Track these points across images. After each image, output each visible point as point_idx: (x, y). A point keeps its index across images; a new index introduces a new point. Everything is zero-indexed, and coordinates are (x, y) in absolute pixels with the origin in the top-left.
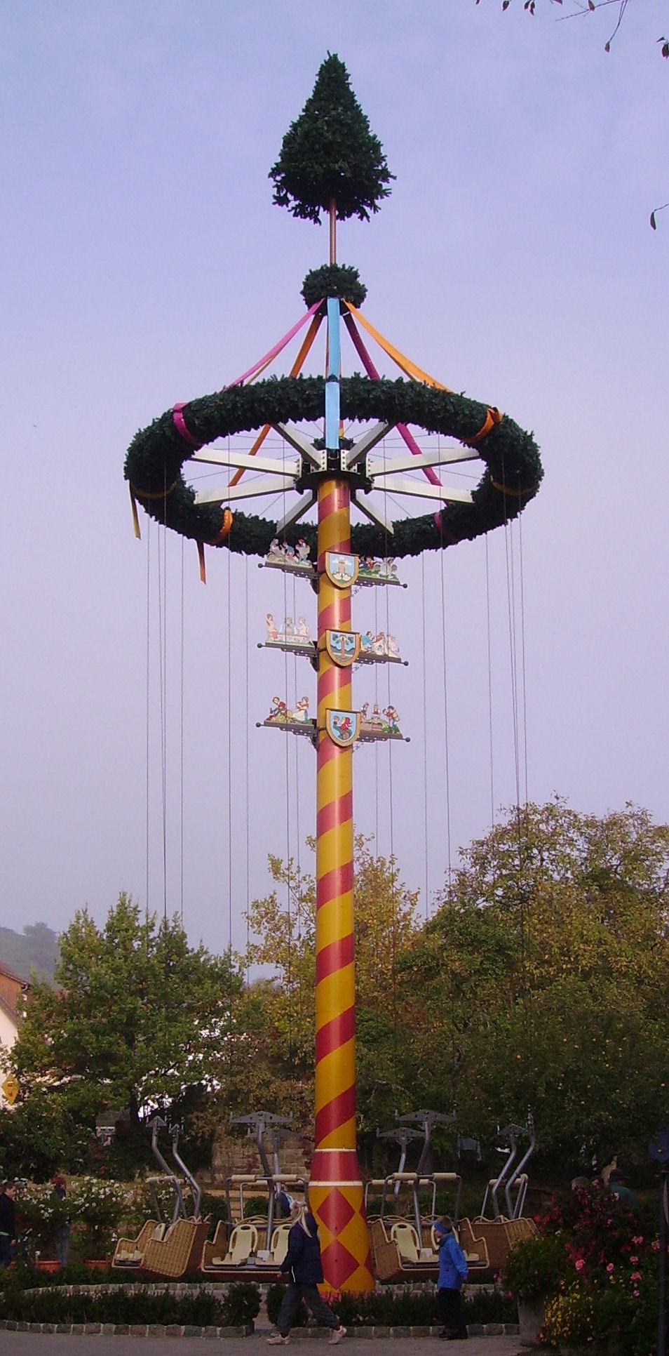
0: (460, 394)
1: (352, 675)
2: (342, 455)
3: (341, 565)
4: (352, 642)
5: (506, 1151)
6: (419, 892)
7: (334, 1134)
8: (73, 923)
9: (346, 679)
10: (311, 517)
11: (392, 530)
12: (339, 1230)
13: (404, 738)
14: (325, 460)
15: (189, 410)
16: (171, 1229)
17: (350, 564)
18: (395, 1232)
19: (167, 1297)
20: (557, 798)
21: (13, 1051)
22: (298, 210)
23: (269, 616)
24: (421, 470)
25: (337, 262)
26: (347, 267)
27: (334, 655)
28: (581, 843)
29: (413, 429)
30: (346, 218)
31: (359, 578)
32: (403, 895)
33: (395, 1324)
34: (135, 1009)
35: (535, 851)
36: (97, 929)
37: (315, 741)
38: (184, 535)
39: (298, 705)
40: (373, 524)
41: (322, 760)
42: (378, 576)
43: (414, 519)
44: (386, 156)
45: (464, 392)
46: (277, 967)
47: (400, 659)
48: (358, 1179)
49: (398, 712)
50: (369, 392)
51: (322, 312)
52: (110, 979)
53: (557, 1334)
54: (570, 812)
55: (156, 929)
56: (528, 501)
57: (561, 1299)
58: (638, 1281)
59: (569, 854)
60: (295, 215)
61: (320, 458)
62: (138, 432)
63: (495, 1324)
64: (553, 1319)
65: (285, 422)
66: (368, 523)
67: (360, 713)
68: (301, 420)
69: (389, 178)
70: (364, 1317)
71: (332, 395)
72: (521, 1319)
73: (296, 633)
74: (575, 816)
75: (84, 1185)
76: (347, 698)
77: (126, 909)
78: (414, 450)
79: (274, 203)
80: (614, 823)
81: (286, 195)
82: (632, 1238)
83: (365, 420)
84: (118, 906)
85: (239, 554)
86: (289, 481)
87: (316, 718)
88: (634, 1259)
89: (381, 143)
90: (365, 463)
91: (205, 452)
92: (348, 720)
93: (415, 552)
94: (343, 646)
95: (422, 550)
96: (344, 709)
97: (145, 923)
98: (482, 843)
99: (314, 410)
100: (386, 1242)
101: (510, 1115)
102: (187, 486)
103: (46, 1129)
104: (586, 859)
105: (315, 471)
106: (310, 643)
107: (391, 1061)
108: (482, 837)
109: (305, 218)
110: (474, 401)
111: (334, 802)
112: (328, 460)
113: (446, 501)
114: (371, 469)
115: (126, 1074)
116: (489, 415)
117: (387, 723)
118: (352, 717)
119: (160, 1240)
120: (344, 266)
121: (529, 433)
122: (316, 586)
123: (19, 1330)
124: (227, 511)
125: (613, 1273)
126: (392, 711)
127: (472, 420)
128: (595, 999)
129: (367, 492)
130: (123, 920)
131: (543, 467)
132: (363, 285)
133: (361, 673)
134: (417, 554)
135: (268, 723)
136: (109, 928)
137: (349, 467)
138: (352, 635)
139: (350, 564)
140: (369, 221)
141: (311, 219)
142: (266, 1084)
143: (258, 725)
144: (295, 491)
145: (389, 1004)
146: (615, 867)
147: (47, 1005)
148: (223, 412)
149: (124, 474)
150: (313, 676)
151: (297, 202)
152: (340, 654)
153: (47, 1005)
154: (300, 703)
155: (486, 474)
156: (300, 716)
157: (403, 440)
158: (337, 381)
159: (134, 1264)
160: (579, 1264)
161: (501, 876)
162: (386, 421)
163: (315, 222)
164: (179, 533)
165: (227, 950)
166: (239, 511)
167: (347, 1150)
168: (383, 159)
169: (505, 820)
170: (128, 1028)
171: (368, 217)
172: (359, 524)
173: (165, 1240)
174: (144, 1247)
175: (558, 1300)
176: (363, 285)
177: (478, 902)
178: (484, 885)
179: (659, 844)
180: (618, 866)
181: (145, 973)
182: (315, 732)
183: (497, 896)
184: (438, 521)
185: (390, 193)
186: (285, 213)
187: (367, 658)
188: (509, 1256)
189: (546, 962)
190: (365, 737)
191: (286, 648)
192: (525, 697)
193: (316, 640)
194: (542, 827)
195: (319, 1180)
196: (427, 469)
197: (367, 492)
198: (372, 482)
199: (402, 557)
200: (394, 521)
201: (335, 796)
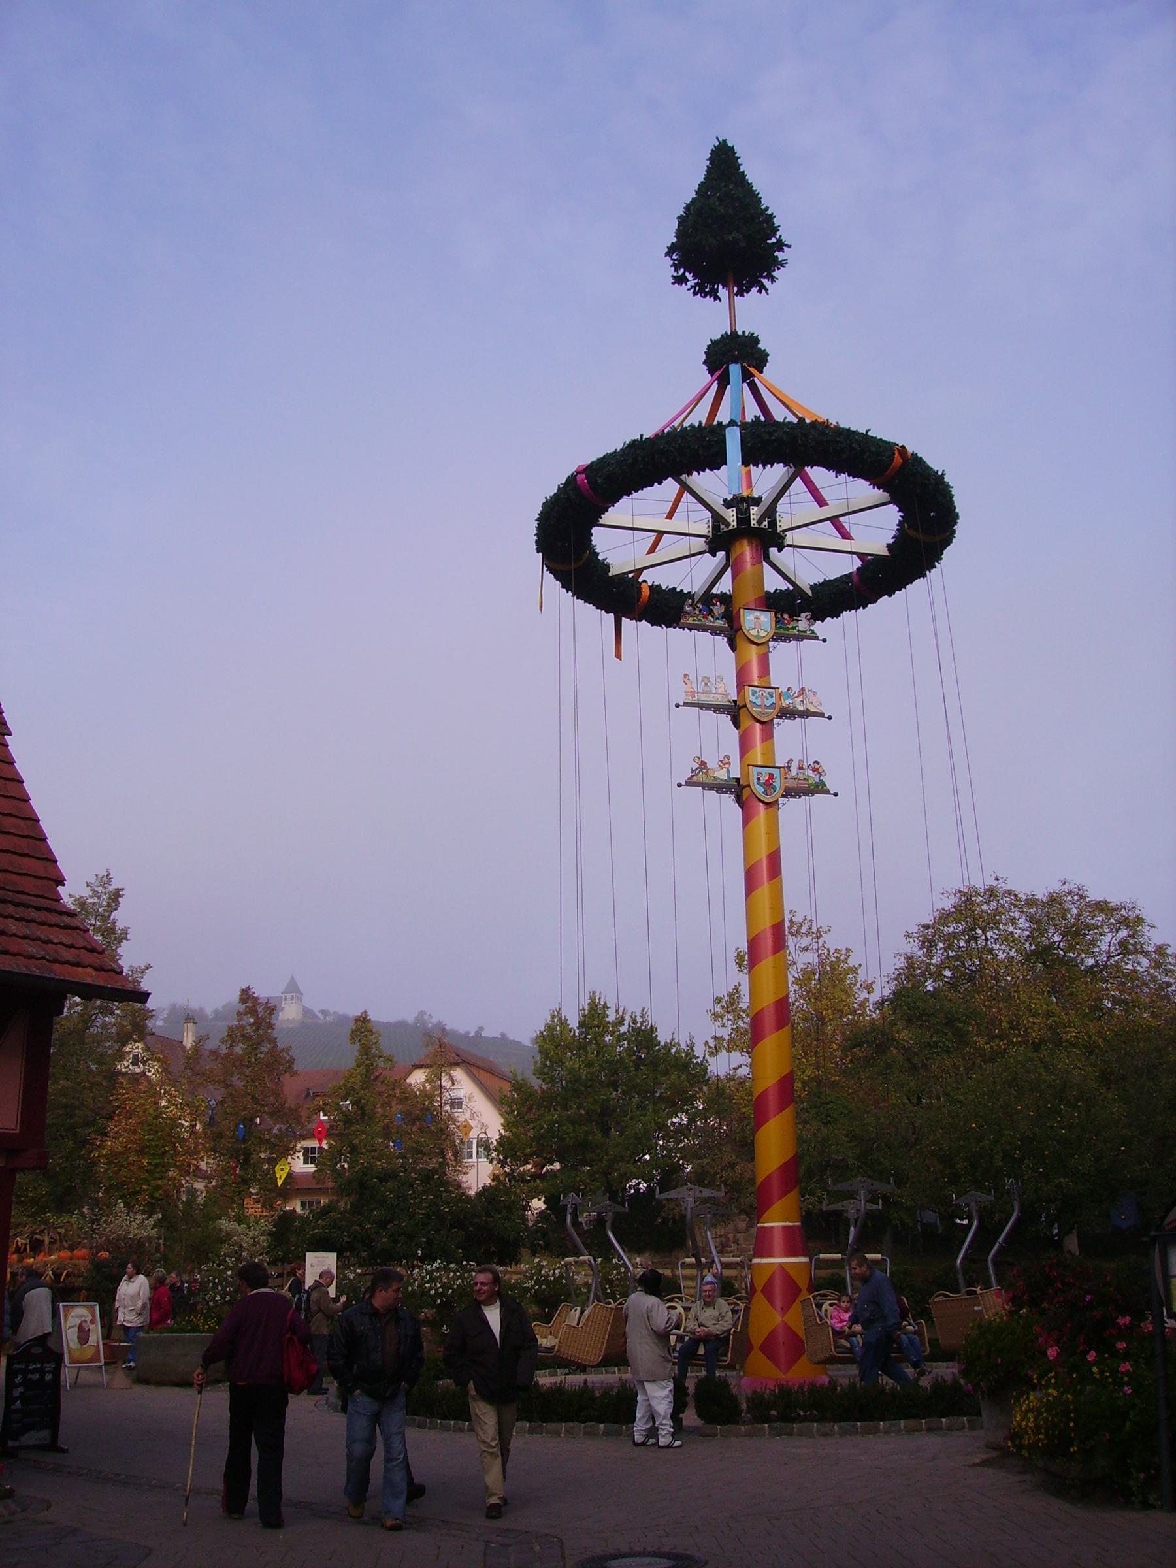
0: (865, 432)
1: (775, 731)
2: (752, 512)
3: (757, 622)
4: (772, 697)
5: (965, 1222)
6: (874, 982)
7: (777, 1208)
8: (548, 1022)
9: (768, 735)
10: (725, 586)
11: (810, 593)
12: (785, 1310)
13: (832, 792)
14: (735, 518)
15: (592, 470)
16: (586, 1312)
17: (766, 620)
18: (826, 1310)
19: (585, 1389)
20: (997, 879)
21: (498, 1143)
22: (697, 288)
23: (686, 675)
24: (829, 522)
25: (737, 329)
26: (747, 334)
27: (755, 711)
28: (1023, 923)
29: (817, 474)
30: (745, 294)
31: (775, 634)
32: (860, 983)
33: (840, 1419)
34: (608, 1100)
35: (979, 931)
36: (570, 1027)
37: (739, 800)
38: (602, 610)
39: (720, 763)
40: (791, 588)
41: (747, 820)
42: (796, 632)
43: (831, 581)
44: (779, 226)
45: (869, 430)
46: (742, 1056)
47: (823, 714)
48: (804, 1255)
49: (825, 766)
50: (771, 434)
51: (724, 381)
52: (584, 1073)
53: (1029, 1443)
54: (1010, 893)
55: (626, 1022)
56: (945, 548)
57: (1031, 1397)
58: (1128, 1373)
59: (1012, 932)
60: (695, 294)
61: (729, 517)
62: (545, 500)
63: (956, 1418)
64: (1024, 1424)
65: (690, 474)
66: (786, 588)
67: (783, 768)
68: (704, 471)
69: (784, 248)
70: (805, 1412)
71: (733, 442)
72: (984, 1414)
73: (714, 692)
74: (1016, 895)
75: (535, 1267)
76: (770, 753)
77: (596, 1006)
78: (821, 502)
79: (673, 283)
80: (1054, 900)
81: (684, 273)
82: (1117, 1317)
83: (769, 466)
84: (589, 1004)
85: (659, 627)
86: (700, 544)
87: (739, 777)
88: (1121, 1345)
89: (774, 214)
90: (775, 520)
91: (613, 515)
92: (771, 776)
93: (836, 614)
94: (763, 701)
95: (842, 613)
96: (768, 765)
97: (614, 1019)
98: (927, 927)
99: (716, 460)
100: (817, 1322)
101: (967, 1185)
102: (600, 557)
103: (504, 1213)
104: (1028, 936)
105: (726, 529)
106: (730, 702)
107: (847, 1136)
108: (928, 920)
109: (705, 297)
110: (881, 439)
111: (761, 859)
112: (737, 518)
113: (861, 556)
114: (783, 523)
115: (601, 1161)
116: (896, 453)
117: (813, 777)
118: (776, 772)
119: (574, 1324)
120: (744, 332)
121: (940, 473)
122: (733, 646)
123: (429, 1429)
124: (644, 584)
125: (1095, 1363)
126: (817, 766)
127: (880, 458)
128: (1046, 1068)
129: (780, 551)
130: (594, 1016)
131: (957, 510)
132: (765, 350)
133: (784, 730)
134: (838, 616)
135: (689, 783)
136: (582, 1025)
137: (760, 522)
138: (773, 690)
139: (766, 620)
140: (768, 294)
141: (710, 297)
142: (732, 1165)
143: (679, 785)
144: (708, 554)
145: (849, 1088)
146: (1057, 943)
147: (526, 1100)
148: (624, 467)
149: (536, 547)
150: (735, 734)
151: (696, 281)
152: (760, 710)
153: (526, 1100)
154: (721, 761)
155: (900, 524)
156: (722, 775)
157: (809, 493)
158: (737, 425)
159: (548, 1350)
160: (1052, 1352)
161: (948, 957)
162: (791, 465)
163: (715, 300)
164: (597, 608)
165: (688, 1042)
166: (656, 584)
167: (791, 1224)
168: (776, 229)
169: (948, 903)
170: (604, 1117)
171: (766, 290)
172: (776, 590)
173: (580, 1325)
174: (558, 1332)
175: (1028, 1398)
176: (765, 350)
177: (926, 984)
178: (932, 967)
179: (1099, 918)
180: (1060, 942)
181: (615, 1067)
182: (738, 790)
183: (945, 976)
184: (855, 579)
185: (786, 263)
186: (684, 291)
187: (788, 713)
188: (966, 1341)
189: (997, 1036)
190: (790, 793)
191: (707, 707)
192: (947, 722)
193: (736, 699)
194: (984, 907)
195: (762, 1256)
196: (834, 520)
197: (780, 551)
198: (784, 538)
199: (822, 621)
200: (812, 584)
201: (762, 853)
